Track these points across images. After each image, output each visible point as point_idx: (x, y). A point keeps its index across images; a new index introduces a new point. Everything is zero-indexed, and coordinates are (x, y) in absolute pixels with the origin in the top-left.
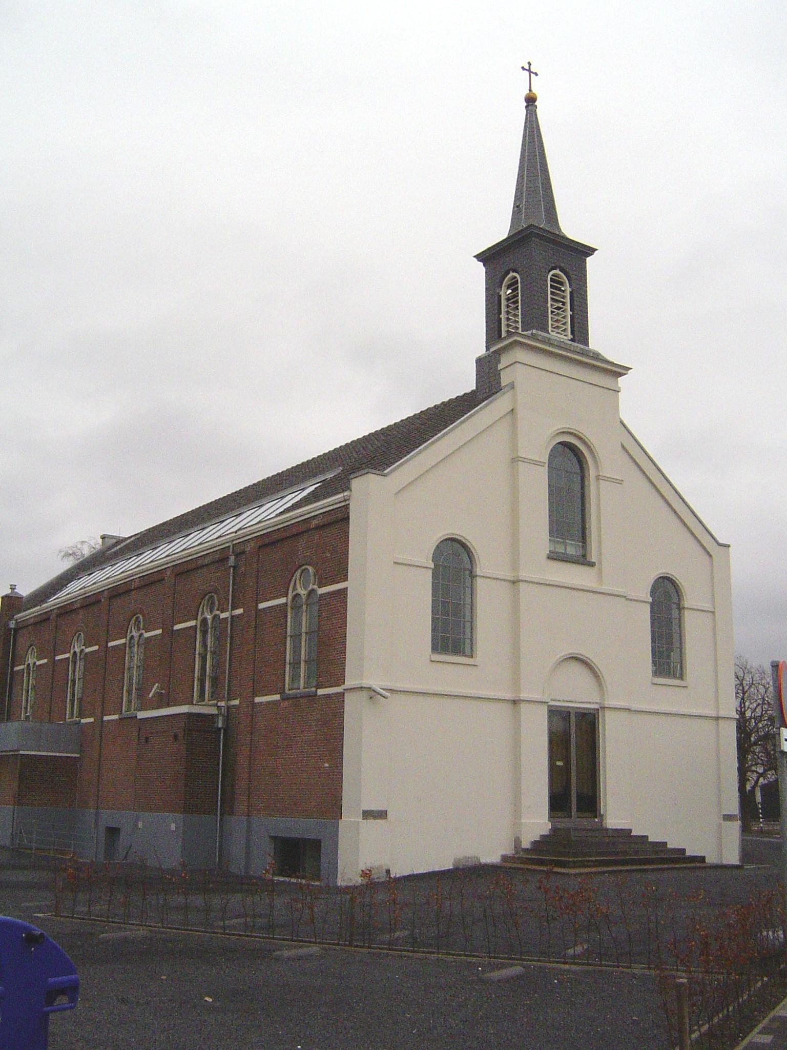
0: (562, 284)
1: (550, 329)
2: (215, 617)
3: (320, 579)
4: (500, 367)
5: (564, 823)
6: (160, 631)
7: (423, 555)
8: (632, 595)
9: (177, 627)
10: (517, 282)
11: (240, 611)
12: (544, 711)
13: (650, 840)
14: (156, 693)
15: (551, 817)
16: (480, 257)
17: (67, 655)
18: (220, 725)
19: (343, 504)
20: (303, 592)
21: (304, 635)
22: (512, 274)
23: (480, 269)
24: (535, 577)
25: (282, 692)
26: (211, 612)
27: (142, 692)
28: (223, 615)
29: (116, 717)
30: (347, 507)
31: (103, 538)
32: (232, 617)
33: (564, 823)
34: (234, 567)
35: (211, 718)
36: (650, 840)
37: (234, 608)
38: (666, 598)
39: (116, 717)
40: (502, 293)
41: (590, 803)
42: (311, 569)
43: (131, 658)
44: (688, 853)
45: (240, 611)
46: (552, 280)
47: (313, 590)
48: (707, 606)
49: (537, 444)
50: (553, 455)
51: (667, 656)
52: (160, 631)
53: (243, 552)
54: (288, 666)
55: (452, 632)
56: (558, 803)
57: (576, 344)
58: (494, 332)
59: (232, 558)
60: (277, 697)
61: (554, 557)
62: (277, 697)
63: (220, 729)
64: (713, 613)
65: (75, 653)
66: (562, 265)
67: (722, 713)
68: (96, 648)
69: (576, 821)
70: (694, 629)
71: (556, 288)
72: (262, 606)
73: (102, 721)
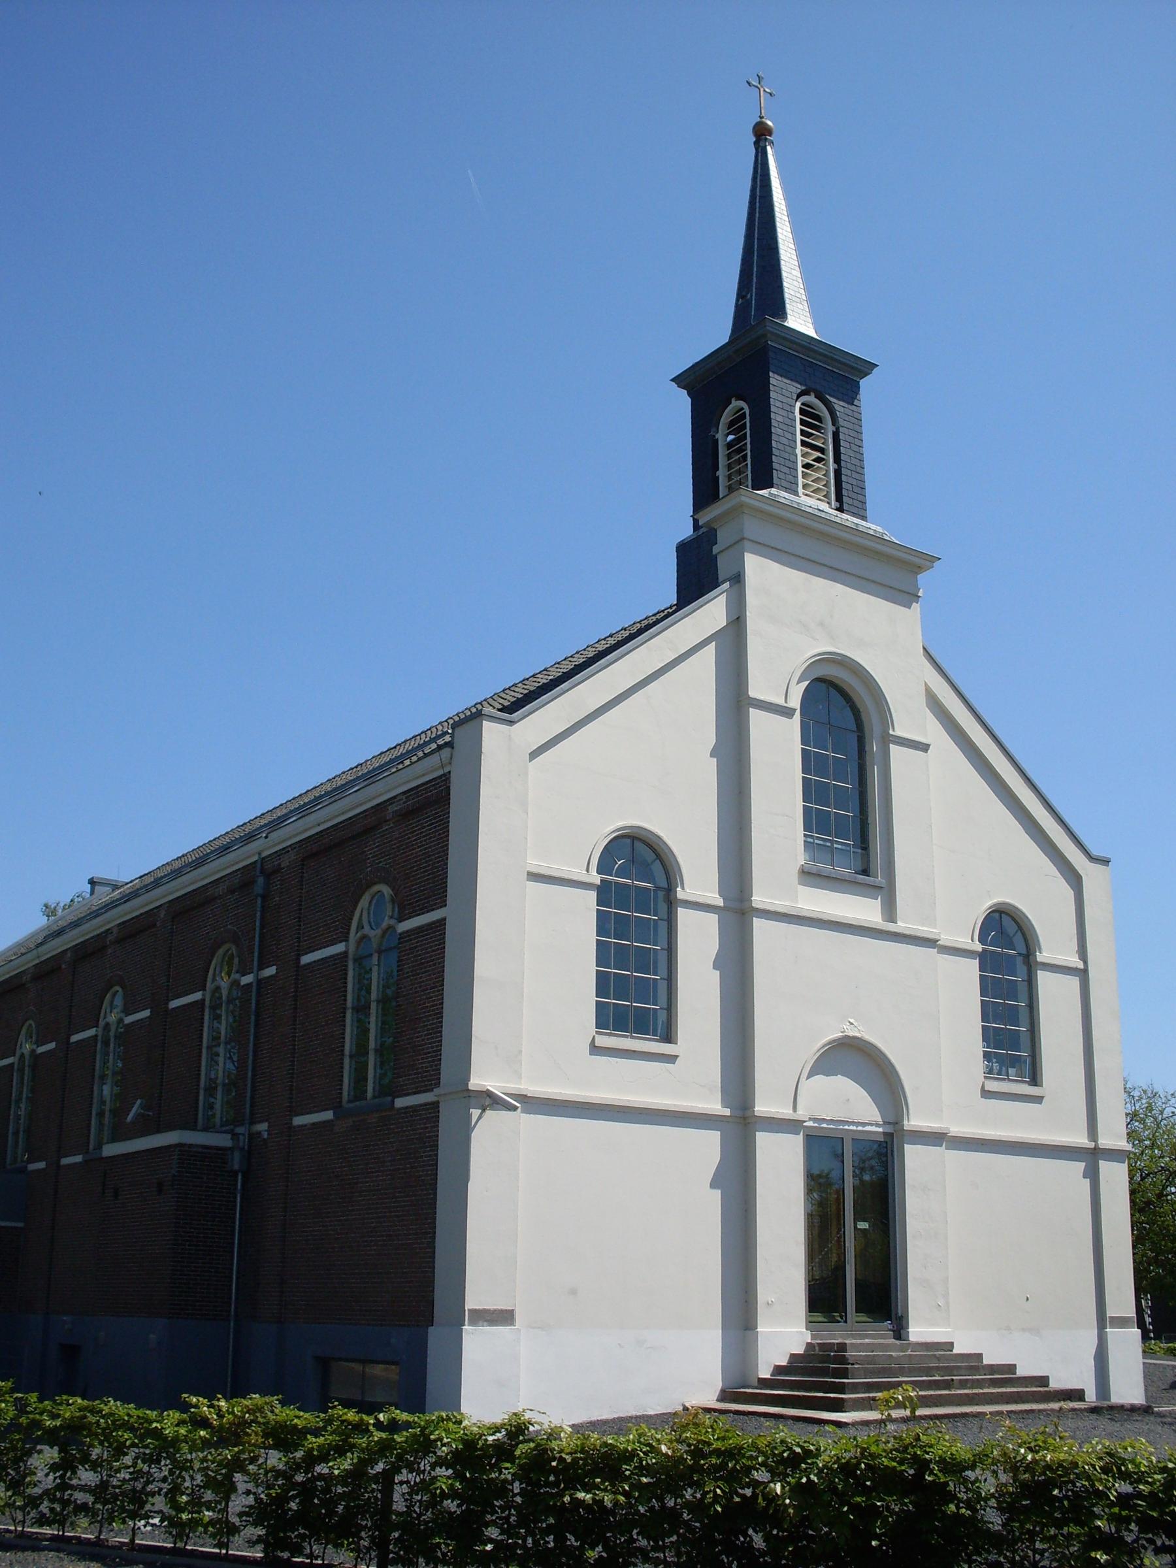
0: (818, 418)
1: (800, 490)
2: (236, 983)
3: (402, 908)
4: (715, 550)
5: (835, 1335)
6: (146, 1013)
7: (579, 859)
8: (945, 939)
9: (174, 1004)
10: (743, 416)
11: (271, 971)
12: (796, 1143)
13: (957, 1350)
14: (138, 1115)
15: (810, 1323)
16: (679, 380)
17: (10, 1060)
18: (236, 1167)
19: (441, 772)
20: (374, 934)
21: (373, 1006)
22: (736, 404)
23: (682, 402)
24: (780, 904)
25: (337, 1107)
26: (229, 974)
27: (119, 1113)
28: (247, 979)
29: (78, 1159)
30: (446, 778)
31: (92, 882)
32: (259, 982)
33: (835, 1335)
34: (264, 897)
35: (220, 1153)
36: (957, 1350)
37: (261, 968)
38: (1006, 946)
39: (78, 1159)
40: (719, 436)
41: (882, 1298)
42: (386, 890)
43: (105, 1062)
44: (1021, 1372)
45: (271, 971)
46: (802, 412)
47: (390, 927)
48: (1075, 961)
49: (777, 674)
50: (808, 698)
51: (1011, 1043)
52: (146, 1013)
53: (278, 870)
54: (347, 1061)
55: (633, 998)
56: (823, 1299)
57: (845, 516)
58: (705, 491)
59: (261, 880)
60: (328, 1115)
61: (809, 876)
62: (328, 1115)
63: (236, 1173)
64: (1083, 974)
65: (22, 1055)
66: (818, 387)
67: (1105, 1142)
68: (52, 1045)
69: (861, 1339)
70: (1055, 997)
71: (809, 435)
72: (306, 959)
73: (58, 1166)
